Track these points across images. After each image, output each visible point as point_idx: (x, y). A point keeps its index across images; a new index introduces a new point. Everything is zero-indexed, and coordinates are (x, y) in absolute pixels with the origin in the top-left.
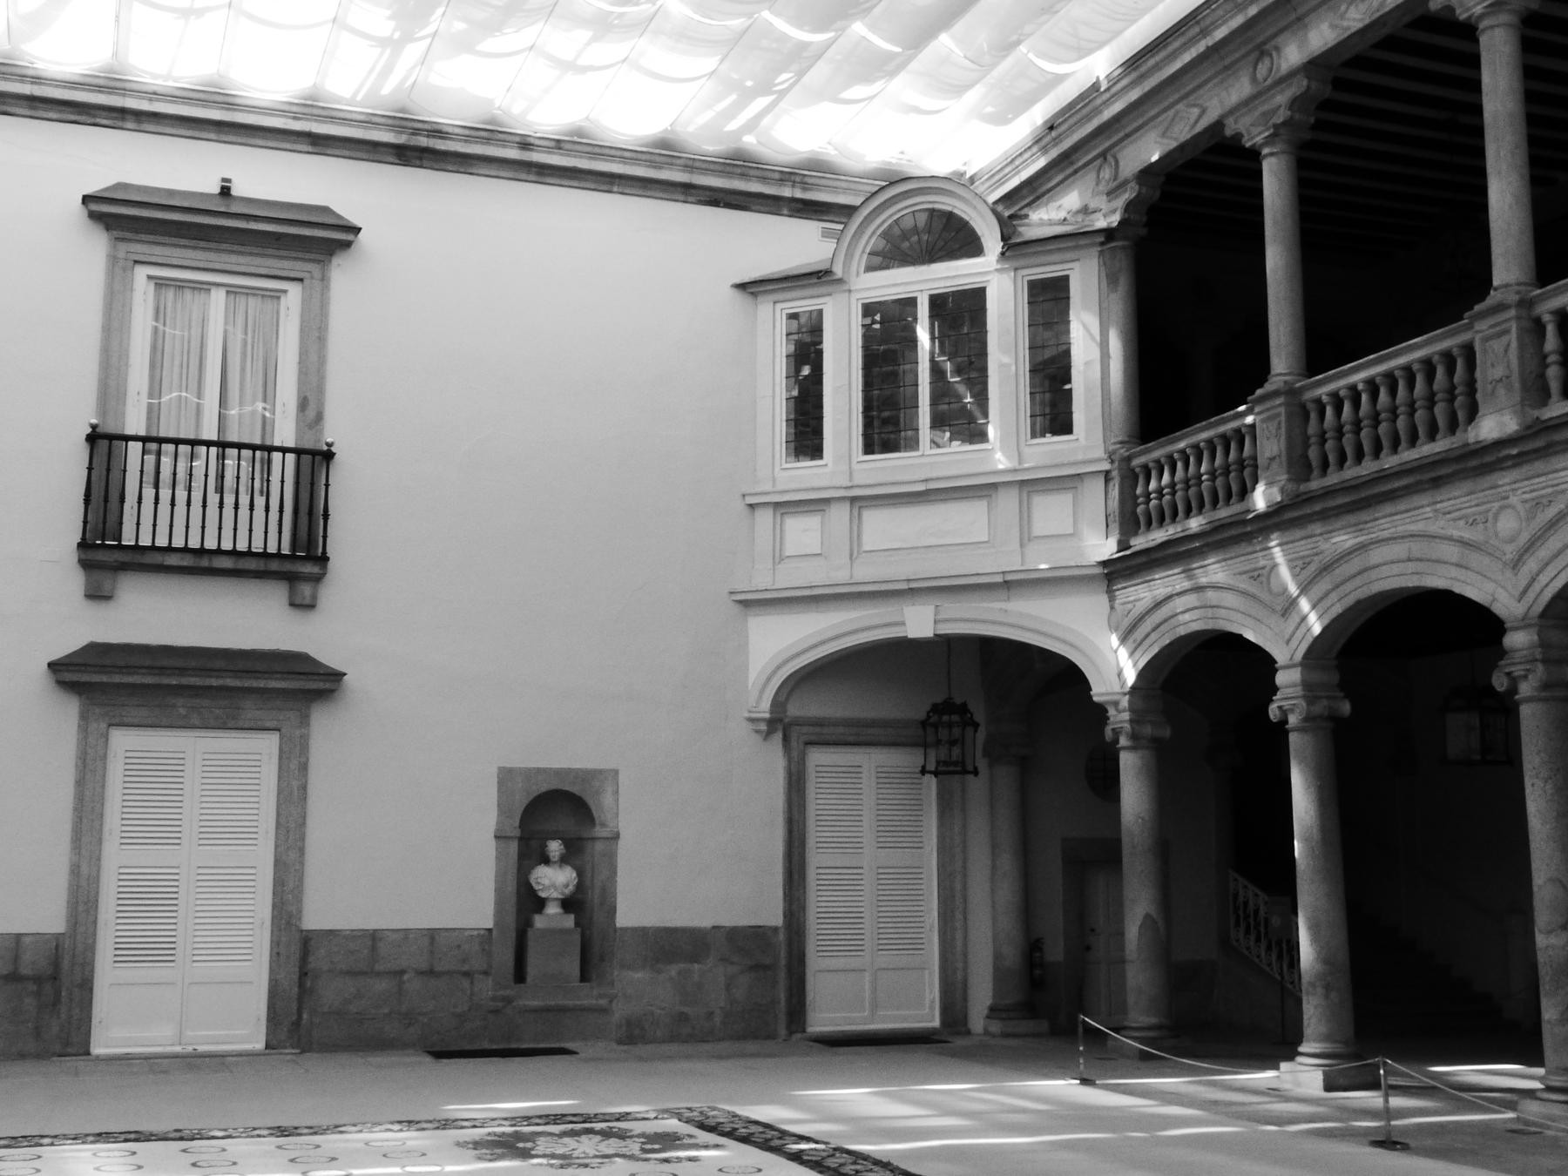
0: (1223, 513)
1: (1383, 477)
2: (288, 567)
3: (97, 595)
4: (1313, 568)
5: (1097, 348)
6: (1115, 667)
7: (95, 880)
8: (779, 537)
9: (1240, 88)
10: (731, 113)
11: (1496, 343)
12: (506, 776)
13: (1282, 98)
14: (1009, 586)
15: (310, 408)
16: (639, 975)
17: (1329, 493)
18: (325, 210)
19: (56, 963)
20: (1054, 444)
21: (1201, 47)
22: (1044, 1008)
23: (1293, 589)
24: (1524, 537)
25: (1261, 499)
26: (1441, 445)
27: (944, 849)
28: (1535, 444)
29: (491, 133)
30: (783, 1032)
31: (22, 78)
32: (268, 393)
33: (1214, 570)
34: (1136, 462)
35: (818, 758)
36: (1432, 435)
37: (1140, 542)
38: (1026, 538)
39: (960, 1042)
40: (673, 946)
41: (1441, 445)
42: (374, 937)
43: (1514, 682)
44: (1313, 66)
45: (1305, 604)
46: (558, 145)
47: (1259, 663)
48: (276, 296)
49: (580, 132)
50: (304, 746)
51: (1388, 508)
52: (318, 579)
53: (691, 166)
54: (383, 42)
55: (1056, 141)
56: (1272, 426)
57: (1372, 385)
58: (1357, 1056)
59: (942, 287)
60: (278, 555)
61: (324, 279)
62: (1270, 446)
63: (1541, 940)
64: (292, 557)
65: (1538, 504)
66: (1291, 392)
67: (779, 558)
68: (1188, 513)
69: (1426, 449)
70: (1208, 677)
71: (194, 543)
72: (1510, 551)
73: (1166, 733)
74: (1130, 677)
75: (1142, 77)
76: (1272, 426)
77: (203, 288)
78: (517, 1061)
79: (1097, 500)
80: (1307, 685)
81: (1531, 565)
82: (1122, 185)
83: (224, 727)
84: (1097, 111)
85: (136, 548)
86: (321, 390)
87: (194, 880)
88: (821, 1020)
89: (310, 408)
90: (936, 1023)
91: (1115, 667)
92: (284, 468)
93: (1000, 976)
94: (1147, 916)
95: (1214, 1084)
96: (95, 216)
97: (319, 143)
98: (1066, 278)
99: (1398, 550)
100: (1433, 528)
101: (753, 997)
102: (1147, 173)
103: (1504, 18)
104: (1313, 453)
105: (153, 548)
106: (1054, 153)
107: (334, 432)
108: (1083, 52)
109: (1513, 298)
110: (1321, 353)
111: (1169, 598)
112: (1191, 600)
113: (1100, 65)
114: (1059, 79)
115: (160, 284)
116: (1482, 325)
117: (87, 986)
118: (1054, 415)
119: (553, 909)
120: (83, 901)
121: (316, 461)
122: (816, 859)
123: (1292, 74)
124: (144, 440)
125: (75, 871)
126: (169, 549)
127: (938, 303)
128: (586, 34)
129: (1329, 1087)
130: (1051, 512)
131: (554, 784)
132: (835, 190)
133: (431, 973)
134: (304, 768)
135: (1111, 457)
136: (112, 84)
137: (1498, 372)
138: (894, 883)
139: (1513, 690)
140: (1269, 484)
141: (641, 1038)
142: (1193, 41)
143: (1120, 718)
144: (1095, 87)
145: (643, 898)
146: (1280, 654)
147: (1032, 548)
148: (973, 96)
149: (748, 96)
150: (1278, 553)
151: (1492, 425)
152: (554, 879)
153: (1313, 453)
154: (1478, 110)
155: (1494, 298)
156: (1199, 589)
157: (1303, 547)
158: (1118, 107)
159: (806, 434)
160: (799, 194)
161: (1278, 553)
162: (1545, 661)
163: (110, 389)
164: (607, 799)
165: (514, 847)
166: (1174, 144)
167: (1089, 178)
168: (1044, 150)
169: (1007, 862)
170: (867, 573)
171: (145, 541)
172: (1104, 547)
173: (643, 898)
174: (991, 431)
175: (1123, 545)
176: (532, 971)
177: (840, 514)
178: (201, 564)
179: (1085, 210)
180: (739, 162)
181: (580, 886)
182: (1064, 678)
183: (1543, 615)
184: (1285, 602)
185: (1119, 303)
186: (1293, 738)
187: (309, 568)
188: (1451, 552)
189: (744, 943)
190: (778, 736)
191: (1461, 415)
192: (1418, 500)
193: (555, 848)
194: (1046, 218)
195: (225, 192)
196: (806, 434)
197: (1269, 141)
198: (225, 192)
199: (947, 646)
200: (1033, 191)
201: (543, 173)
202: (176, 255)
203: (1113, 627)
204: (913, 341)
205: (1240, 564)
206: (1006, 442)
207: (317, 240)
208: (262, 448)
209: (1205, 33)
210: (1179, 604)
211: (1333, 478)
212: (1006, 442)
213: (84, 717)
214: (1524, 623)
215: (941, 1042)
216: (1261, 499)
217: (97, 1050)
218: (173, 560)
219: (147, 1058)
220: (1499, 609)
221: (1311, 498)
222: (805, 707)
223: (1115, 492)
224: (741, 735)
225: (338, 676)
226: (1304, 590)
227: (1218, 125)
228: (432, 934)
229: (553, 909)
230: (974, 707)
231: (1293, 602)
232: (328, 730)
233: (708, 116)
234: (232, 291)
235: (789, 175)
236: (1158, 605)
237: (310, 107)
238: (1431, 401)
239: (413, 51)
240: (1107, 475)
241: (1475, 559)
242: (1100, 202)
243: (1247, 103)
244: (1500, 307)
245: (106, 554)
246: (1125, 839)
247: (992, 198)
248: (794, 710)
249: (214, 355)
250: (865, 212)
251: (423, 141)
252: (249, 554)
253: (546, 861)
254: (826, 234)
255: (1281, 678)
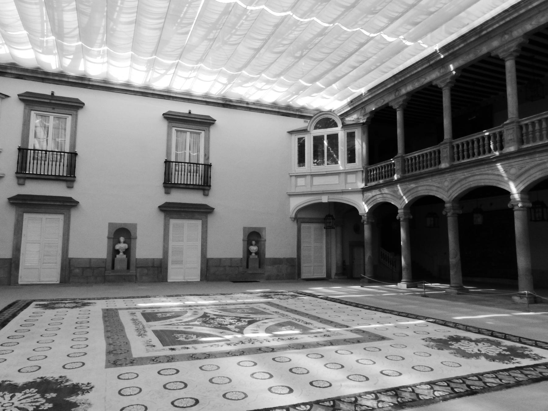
0: (387, 179)
1: (421, 174)
2: (203, 187)
3: (167, 193)
4: (406, 191)
5: (360, 146)
6: (364, 208)
7: (168, 248)
8: (296, 182)
9: (392, 97)
10: (289, 98)
11: (445, 151)
12: (245, 229)
13: (401, 100)
14: (343, 192)
15: (207, 157)
16: (269, 267)
17: (410, 177)
18: (209, 116)
19: (161, 264)
20: (352, 165)
21: (385, 88)
22: (347, 274)
23: (402, 194)
24: (450, 186)
25: (396, 177)
26: (433, 168)
27: (327, 243)
28: (452, 169)
29: (241, 101)
30: (296, 277)
31: (151, 90)
32: (198, 151)
33: (385, 190)
34: (369, 169)
35: (303, 225)
36: (431, 166)
37: (369, 184)
38: (346, 183)
39: (330, 280)
40: (276, 261)
41: (433, 168)
42: (220, 260)
43: (447, 213)
44: (408, 94)
45: (404, 197)
46: (254, 104)
47: (395, 209)
48: (199, 134)
49: (258, 101)
50: (207, 222)
51: (422, 180)
52: (209, 190)
53: (279, 108)
54: (224, 84)
55: (352, 105)
56: (398, 163)
57: (419, 156)
58: (412, 282)
59: (329, 133)
60: (201, 185)
61: (209, 131)
62: (397, 167)
63: (451, 260)
64: (204, 186)
65: (453, 180)
66: (402, 157)
67: (296, 186)
68: (380, 179)
69: (430, 169)
70: (383, 212)
71: (185, 183)
72: (447, 189)
73: (374, 221)
74: (367, 210)
75: (372, 93)
76: (398, 163)
77: (186, 132)
78: (242, 283)
79: (360, 176)
80: (404, 213)
81: (451, 191)
82: (366, 114)
83: (192, 219)
84: (362, 99)
85: (175, 183)
86: (209, 152)
87: (41, 247)
88: (304, 276)
89: (207, 157)
90: (325, 276)
91: (364, 208)
92: (201, 168)
93: (337, 267)
94: (370, 256)
95: (372, 288)
96: (165, 118)
97: (208, 103)
98: (354, 132)
99: (424, 188)
100: (431, 184)
101: (290, 272)
102: (372, 112)
103: (447, 88)
104: (406, 169)
105: (178, 184)
106: (352, 107)
107: (211, 161)
108: (360, 88)
109: (448, 141)
110: (408, 149)
111: (375, 196)
112: (380, 196)
113: (363, 90)
114: (355, 93)
115: (177, 131)
116: (442, 146)
117: (166, 269)
118: (351, 158)
119: (253, 254)
120: (166, 252)
121: (208, 166)
122: (303, 245)
123: (403, 95)
124: (175, 162)
125: (164, 246)
126: (181, 184)
127: (329, 137)
128: (264, 84)
129: (407, 287)
130: (351, 178)
131: (252, 231)
132: (307, 113)
133: (231, 266)
134: (207, 227)
135: (363, 167)
136: (169, 91)
137: (445, 155)
138: (317, 250)
139: (446, 214)
140: (397, 174)
141: (271, 279)
142: (384, 87)
143: (365, 218)
144: (362, 95)
145: (270, 252)
146: (399, 206)
147: (347, 185)
148: (336, 96)
149: (293, 95)
150: (399, 188)
151: (443, 165)
152: (254, 248)
153: (406, 169)
154: (442, 106)
155: (444, 141)
156: (382, 194)
157: (404, 187)
158: (366, 99)
159: (301, 160)
160: (300, 114)
161: (399, 188)
162: (453, 209)
163: (168, 153)
164: (263, 233)
165: (246, 242)
166: (377, 107)
167: (359, 113)
168: (350, 106)
169: (339, 245)
170: (314, 189)
171: (176, 182)
172: (362, 185)
173: (270, 252)
174: (339, 162)
175: (366, 185)
176: (250, 266)
177: (309, 178)
178: (187, 187)
179: (358, 119)
180: (289, 107)
181: (258, 250)
182: (353, 210)
183: (453, 201)
184: (401, 197)
185: (365, 137)
186: (401, 223)
187: (207, 188)
188: (435, 189)
189: (290, 261)
190: (296, 221)
191: (437, 163)
192: (428, 179)
193: (254, 242)
194: (350, 119)
195: (190, 113)
196: (301, 160)
197: (398, 108)
198: (190, 113)
199: (329, 204)
200: (347, 114)
201: (251, 109)
202: (180, 125)
203: (363, 201)
204: (323, 144)
205: (391, 189)
206: (342, 164)
207: (207, 123)
208: (197, 164)
209: (386, 86)
210: (378, 197)
211: (410, 174)
212: (342, 164)
213: (165, 217)
214: (449, 202)
215: (326, 280)
216: (396, 177)
217: (169, 281)
218: (181, 186)
219: (178, 282)
220: (444, 199)
221: (406, 178)
222: (302, 215)
223: (364, 174)
224: (289, 221)
225: (213, 209)
226: (404, 195)
227: (388, 104)
228: (231, 259)
229: (253, 254)
230: (334, 216)
231: (402, 197)
232: (75, 214)
233: (285, 98)
234: (191, 133)
235: (299, 110)
236: (373, 197)
237: (206, 96)
238: (431, 160)
239: (229, 86)
240: (362, 171)
241: (440, 190)
242: (362, 117)
243: (395, 100)
244: (446, 143)
245: (169, 185)
246: (365, 241)
247: (339, 115)
248: (299, 216)
249: (188, 146)
250: (313, 119)
251: (228, 103)
252: (196, 185)
253: (252, 245)
254: (305, 122)
255: (399, 211)
